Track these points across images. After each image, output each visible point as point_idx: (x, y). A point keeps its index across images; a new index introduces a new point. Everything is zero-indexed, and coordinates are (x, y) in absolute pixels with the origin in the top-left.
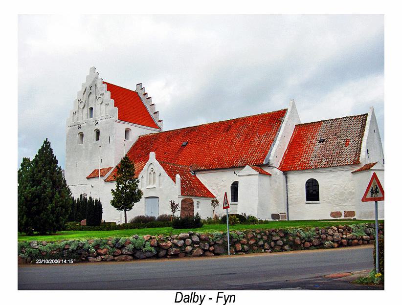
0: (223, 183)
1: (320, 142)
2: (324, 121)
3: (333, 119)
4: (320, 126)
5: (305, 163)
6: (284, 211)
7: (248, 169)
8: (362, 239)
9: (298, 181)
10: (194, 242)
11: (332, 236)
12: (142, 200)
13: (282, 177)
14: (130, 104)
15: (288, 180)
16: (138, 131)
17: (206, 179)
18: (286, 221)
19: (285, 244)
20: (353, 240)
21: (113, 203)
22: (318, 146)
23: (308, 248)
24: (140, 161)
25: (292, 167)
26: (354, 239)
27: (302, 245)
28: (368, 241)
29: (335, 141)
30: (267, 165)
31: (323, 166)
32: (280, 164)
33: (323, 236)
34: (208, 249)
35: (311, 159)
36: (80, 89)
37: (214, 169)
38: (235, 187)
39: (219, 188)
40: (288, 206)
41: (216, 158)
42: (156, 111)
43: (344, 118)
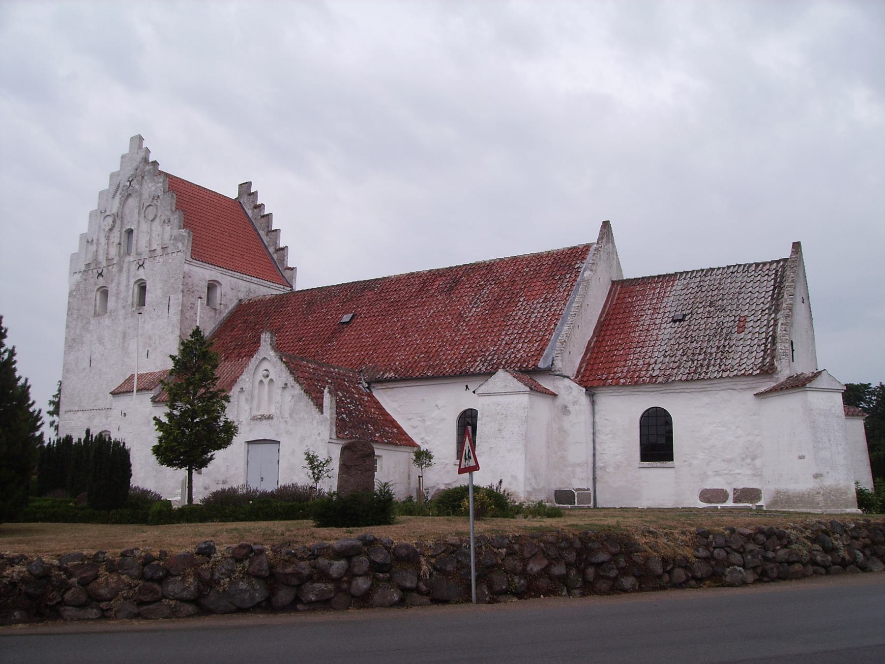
0: (438, 412)
1: (674, 321)
2: (682, 273)
3: (702, 270)
4: (673, 286)
5: (641, 370)
6: (587, 485)
7: (503, 379)
8: (814, 563)
9: (623, 412)
10: (376, 567)
11: (740, 553)
12: (238, 441)
13: (584, 400)
14: (227, 228)
15: (597, 408)
16: (237, 288)
17: (397, 403)
18: (589, 508)
19: (623, 572)
20: (790, 563)
21: (157, 450)
22: (668, 331)
23: (680, 586)
24: (239, 355)
25: (607, 379)
26: (793, 563)
27: (666, 577)
28: (825, 567)
29: (710, 320)
30: (548, 371)
31: (684, 378)
32: (578, 372)
33: (719, 553)
34: (414, 585)
35: (653, 361)
36: (104, 184)
37: (417, 379)
38: (468, 422)
39: (428, 423)
40: (594, 471)
41: (422, 353)
42: (282, 246)
43: (729, 267)
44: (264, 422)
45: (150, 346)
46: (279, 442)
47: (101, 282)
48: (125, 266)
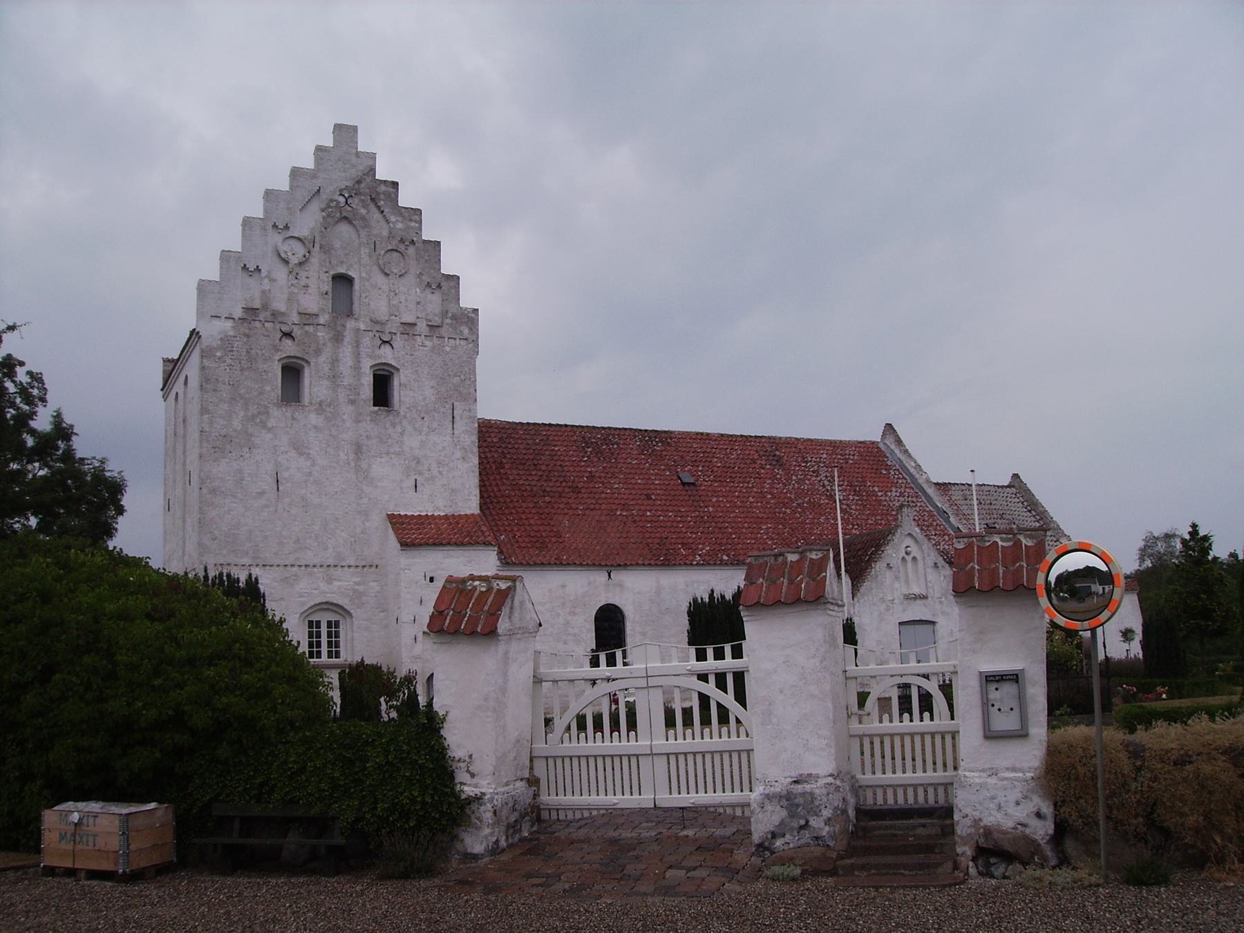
44: (918, 601)
45: (420, 473)
46: (933, 623)
47: (290, 348)
48: (348, 336)
